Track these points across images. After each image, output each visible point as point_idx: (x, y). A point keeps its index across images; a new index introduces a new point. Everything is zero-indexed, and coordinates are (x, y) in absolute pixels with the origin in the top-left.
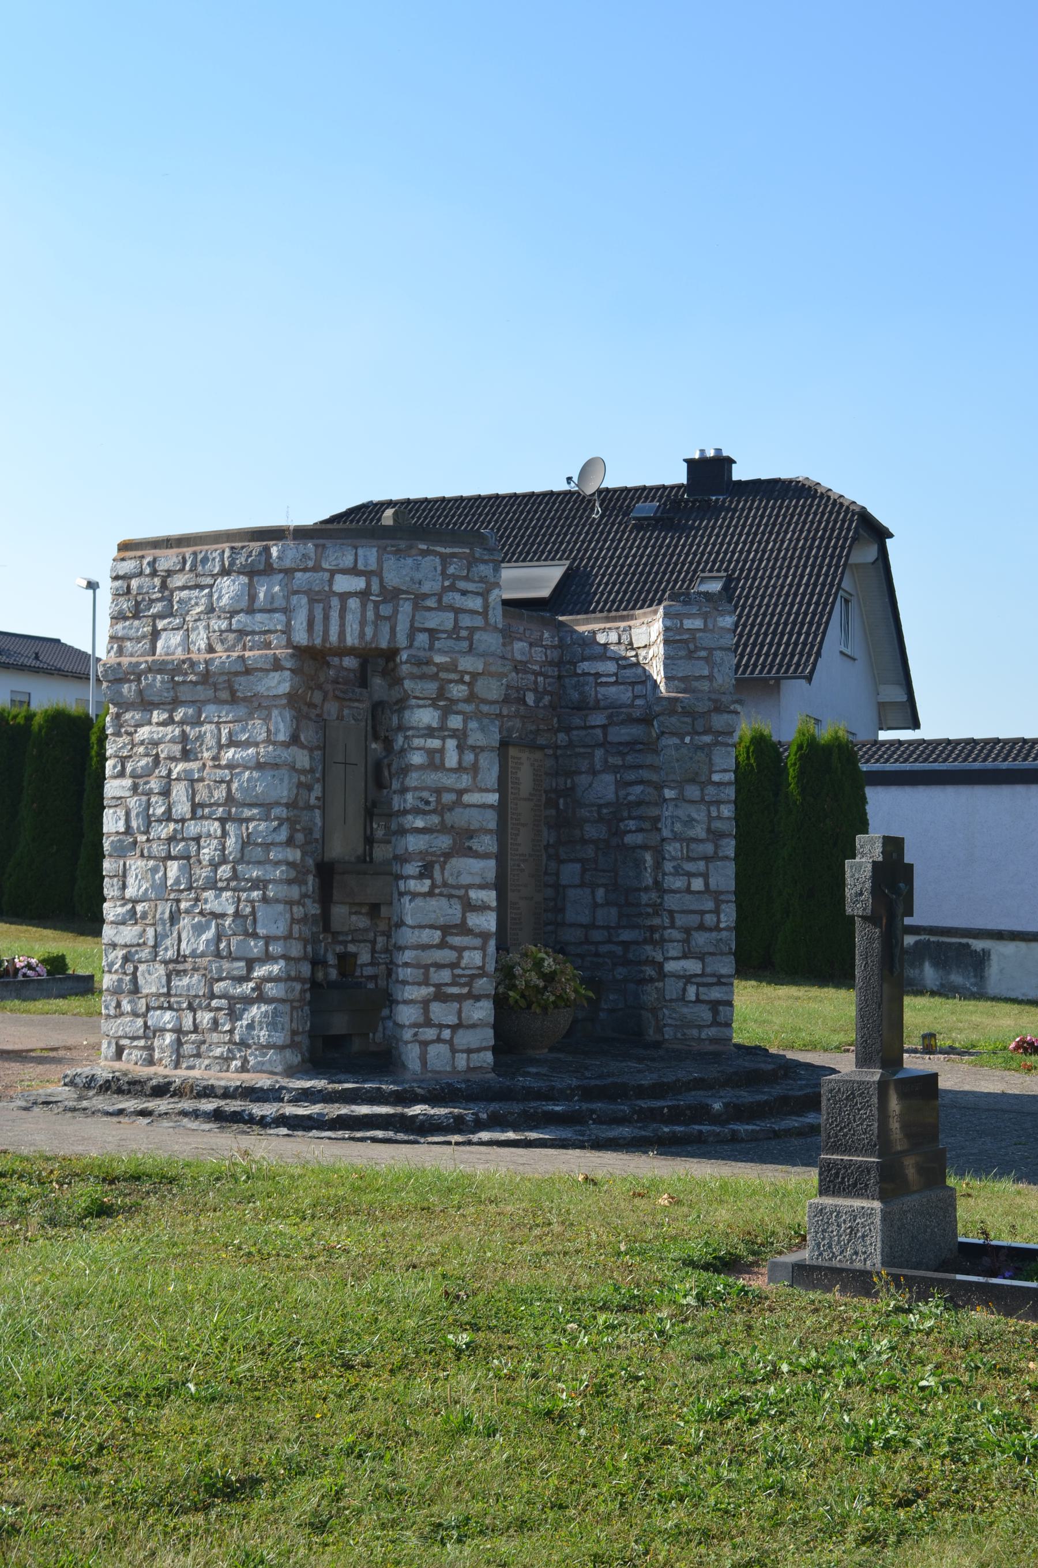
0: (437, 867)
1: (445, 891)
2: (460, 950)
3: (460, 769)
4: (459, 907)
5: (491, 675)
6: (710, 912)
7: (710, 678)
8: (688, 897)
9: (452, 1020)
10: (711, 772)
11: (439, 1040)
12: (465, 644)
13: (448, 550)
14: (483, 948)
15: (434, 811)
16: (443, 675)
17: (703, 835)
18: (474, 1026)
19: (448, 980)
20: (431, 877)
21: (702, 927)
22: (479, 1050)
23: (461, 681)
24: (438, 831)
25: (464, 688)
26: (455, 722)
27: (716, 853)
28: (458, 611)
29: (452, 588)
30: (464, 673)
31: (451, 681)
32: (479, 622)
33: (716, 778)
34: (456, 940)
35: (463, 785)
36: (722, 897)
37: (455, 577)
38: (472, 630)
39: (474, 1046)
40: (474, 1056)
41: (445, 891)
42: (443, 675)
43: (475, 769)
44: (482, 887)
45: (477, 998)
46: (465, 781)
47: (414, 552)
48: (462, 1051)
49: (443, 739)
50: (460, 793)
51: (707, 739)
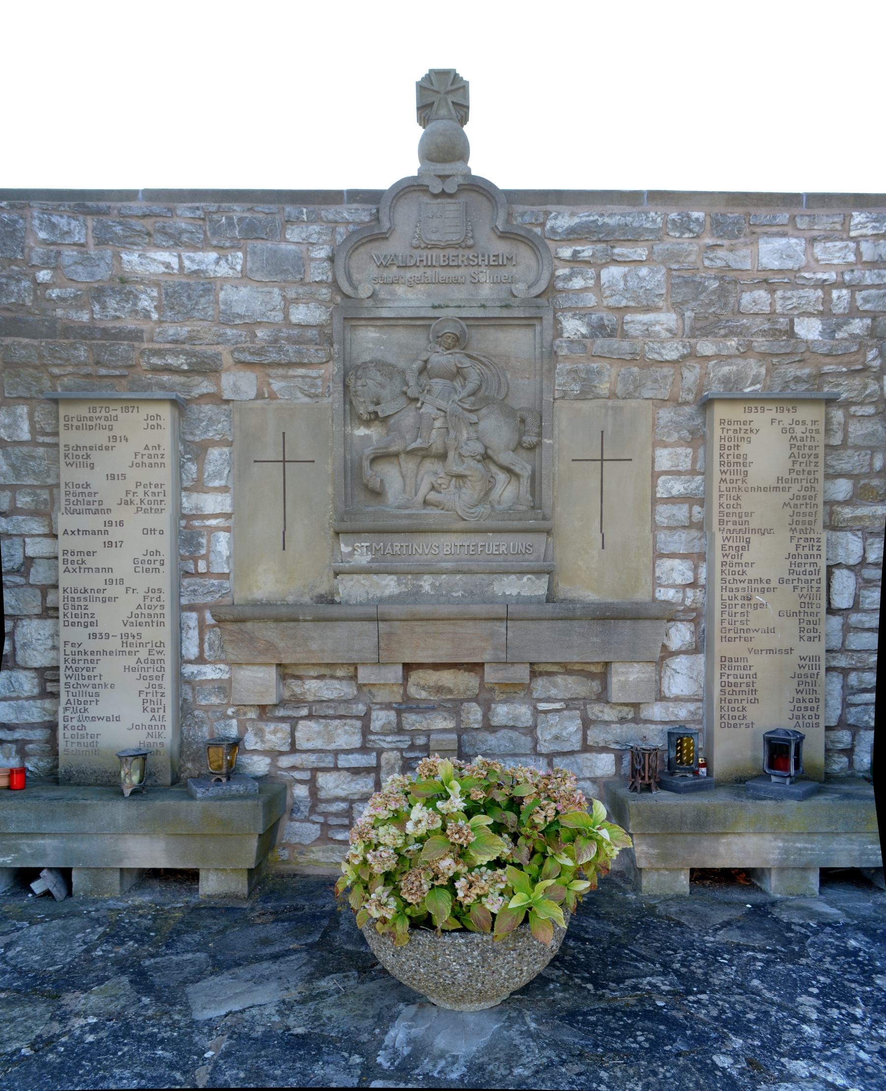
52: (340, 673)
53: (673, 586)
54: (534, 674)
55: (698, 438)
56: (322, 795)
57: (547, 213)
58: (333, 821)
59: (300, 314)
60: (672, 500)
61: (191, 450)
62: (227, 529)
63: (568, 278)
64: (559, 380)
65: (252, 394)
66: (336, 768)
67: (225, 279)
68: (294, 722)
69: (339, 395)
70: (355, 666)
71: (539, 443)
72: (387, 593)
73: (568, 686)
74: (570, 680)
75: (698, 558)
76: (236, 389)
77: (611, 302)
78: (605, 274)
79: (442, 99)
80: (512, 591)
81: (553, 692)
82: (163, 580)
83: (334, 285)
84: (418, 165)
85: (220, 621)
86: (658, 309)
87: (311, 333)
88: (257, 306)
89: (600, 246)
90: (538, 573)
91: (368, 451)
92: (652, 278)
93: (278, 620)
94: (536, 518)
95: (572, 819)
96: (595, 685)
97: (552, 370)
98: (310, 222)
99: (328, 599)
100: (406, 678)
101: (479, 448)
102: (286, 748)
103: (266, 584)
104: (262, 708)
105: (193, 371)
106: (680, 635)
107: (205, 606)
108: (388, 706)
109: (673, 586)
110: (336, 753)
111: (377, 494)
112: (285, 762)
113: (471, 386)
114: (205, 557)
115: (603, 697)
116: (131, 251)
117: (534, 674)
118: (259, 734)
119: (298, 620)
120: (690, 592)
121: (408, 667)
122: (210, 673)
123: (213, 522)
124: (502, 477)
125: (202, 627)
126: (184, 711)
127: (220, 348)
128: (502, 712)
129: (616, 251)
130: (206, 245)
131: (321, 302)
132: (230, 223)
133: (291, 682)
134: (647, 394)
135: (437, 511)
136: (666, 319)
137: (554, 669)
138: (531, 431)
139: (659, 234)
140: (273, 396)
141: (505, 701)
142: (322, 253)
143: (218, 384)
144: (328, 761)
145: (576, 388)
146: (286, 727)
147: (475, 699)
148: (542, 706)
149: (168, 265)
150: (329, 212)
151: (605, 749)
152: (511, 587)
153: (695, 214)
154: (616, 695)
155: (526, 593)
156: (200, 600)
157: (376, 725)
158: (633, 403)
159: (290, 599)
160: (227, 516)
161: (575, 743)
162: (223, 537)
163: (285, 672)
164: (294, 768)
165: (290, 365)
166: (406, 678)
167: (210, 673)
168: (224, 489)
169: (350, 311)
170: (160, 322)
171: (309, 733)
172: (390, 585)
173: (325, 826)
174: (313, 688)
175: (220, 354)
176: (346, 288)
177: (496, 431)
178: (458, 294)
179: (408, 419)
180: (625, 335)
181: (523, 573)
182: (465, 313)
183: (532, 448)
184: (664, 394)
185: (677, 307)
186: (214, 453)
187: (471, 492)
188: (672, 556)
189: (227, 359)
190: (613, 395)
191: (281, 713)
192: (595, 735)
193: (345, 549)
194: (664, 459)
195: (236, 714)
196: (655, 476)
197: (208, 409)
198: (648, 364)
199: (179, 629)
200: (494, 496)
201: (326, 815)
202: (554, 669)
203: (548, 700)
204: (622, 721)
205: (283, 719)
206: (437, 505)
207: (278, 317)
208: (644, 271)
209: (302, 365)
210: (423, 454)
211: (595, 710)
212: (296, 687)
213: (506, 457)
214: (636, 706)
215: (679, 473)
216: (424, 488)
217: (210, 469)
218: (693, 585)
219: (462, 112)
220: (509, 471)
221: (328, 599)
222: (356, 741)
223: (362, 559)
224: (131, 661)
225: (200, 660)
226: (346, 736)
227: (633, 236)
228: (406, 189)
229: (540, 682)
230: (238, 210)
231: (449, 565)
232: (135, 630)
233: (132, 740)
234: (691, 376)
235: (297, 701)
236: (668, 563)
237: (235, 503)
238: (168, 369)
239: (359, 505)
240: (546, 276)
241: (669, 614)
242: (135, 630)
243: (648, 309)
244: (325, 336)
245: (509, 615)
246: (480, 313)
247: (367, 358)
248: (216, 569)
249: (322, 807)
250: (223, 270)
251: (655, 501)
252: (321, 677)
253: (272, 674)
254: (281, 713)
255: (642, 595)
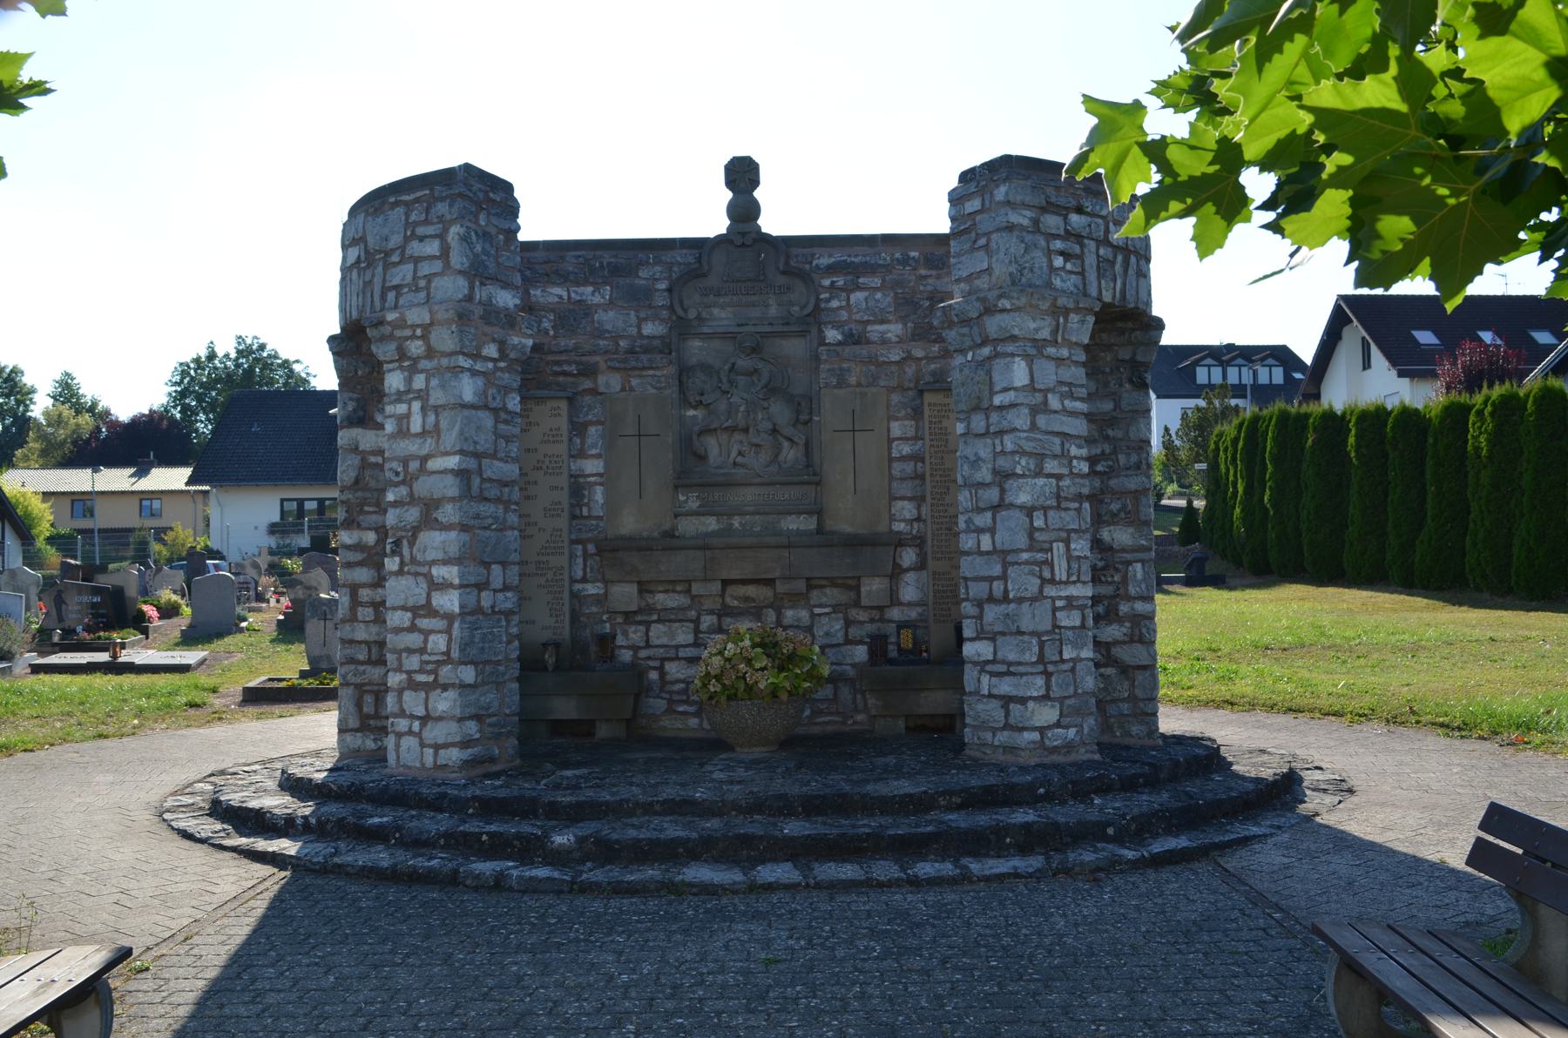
0: (405, 542)
1: (414, 569)
2: (427, 633)
3: (424, 434)
4: (425, 586)
5: (441, 324)
6: (998, 578)
7: (989, 271)
8: (979, 560)
9: (420, 711)
10: (992, 393)
11: (410, 732)
12: (423, 295)
13: (412, 197)
14: (448, 631)
15: (403, 482)
16: (398, 333)
17: (989, 478)
18: (440, 719)
19: (416, 666)
20: (402, 556)
21: (991, 599)
22: (446, 746)
23: (413, 337)
24: (409, 504)
25: (420, 343)
26: (419, 382)
27: (1002, 499)
28: (417, 260)
29: (414, 236)
30: (414, 327)
31: (407, 338)
32: (437, 266)
33: (997, 400)
34: (424, 623)
35: (424, 452)
36: (1009, 559)
37: (417, 224)
38: (429, 278)
39: (440, 741)
40: (442, 752)
41: (414, 569)
42: (398, 333)
43: (437, 430)
44: (446, 562)
45: (445, 688)
46: (428, 446)
47: (387, 207)
48: (430, 746)
49: (409, 402)
50: (424, 459)
51: (986, 351)
52: (679, 588)
53: (904, 520)
54: (810, 587)
55: (917, 414)
56: (668, 678)
57: (813, 255)
58: (676, 697)
59: (649, 329)
60: (903, 458)
61: (578, 429)
62: (601, 484)
63: (828, 300)
64: (823, 375)
65: (618, 388)
66: (678, 658)
67: (598, 305)
68: (648, 624)
69: (676, 389)
70: (689, 582)
71: (811, 420)
72: (710, 529)
73: (833, 595)
74: (835, 590)
75: (919, 500)
76: (607, 385)
77: (857, 317)
78: (853, 297)
79: (742, 174)
80: (793, 526)
81: (824, 600)
82: (563, 522)
83: (671, 308)
84: (728, 222)
85: (600, 552)
86: (889, 322)
87: (657, 343)
88: (620, 324)
89: (849, 277)
90: (810, 513)
91: (696, 429)
92: (884, 299)
93: (639, 549)
94: (811, 474)
95: (801, 651)
96: (852, 594)
97: (817, 370)
98: (655, 263)
99: (670, 534)
100: (724, 591)
101: (769, 426)
102: (642, 644)
103: (629, 524)
104: (627, 615)
105: (581, 374)
106: (908, 557)
107: (588, 541)
108: (711, 612)
109: (904, 520)
110: (677, 647)
111: (702, 458)
112: (643, 654)
113: (764, 381)
114: (587, 505)
115: (857, 604)
116: (536, 288)
117: (810, 587)
118: (625, 633)
119: (651, 549)
120: (915, 525)
121: (726, 583)
122: (592, 589)
123: (592, 479)
124: (786, 444)
125: (586, 556)
126: (575, 617)
127: (598, 358)
128: (789, 615)
129: (861, 280)
130: (586, 283)
131: (662, 320)
132: (602, 267)
133: (647, 596)
134: (882, 383)
135: (742, 471)
136: (894, 330)
137: (824, 582)
138: (804, 408)
139: (888, 268)
140: (632, 389)
141: (792, 607)
142: (663, 286)
143: (595, 381)
144: (672, 653)
145: (834, 381)
146: (642, 628)
147: (771, 606)
148: (817, 611)
149: (560, 297)
150: (668, 257)
151: (861, 642)
152: (792, 524)
153: (913, 254)
154: (865, 601)
155: (802, 527)
156: (584, 536)
157: (704, 626)
158: (874, 390)
159: (645, 534)
160: (600, 475)
161: (840, 638)
162: (599, 490)
163: (644, 588)
164: (649, 658)
165: (644, 368)
166: (724, 591)
167: (592, 589)
168: (598, 456)
169: (682, 328)
170: (555, 337)
171: (658, 633)
172: (712, 524)
173: (671, 701)
174: (662, 599)
175: (597, 363)
176: (680, 312)
177: (780, 412)
178: (755, 313)
179: (722, 406)
180: (868, 342)
181: (801, 513)
182: (759, 329)
183: (806, 423)
184: (894, 383)
185: (903, 319)
186: (592, 430)
187: (764, 457)
188: (902, 498)
189: (603, 366)
190: (859, 385)
191: (639, 618)
192: (854, 632)
193: (682, 498)
194: (896, 429)
195: (609, 619)
196: (890, 441)
197: (588, 399)
198: (880, 365)
199: (572, 556)
200: (781, 458)
201: (671, 693)
202: (824, 582)
203: (820, 606)
204: (872, 621)
205: (640, 623)
206: (743, 466)
207: (633, 331)
208: (879, 295)
209: (651, 368)
210: (732, 429)
211: (854, 613)
212: (650, 599)
213: (788, 431)
214: (881, 609)
215: (907, 439)
216: (734, 454)
217: (589, 441)
218: (918, 519)
219: (755, 183)
220: (790, 440)
221: (670, 534)
222: (690, 638)
223: (693, 504)
224: (542, 581)
225: (584, 580)
226: (684, 636)
227: (870, 269)
228: (720, 239)
229: (815, 593)
230: (607, 257)
231: (751, 509)
232: (545, 559)
233: (546, 636)
234: (910, 370)
235: (650, 609)
236: (900, 504)
237: (606, 467)
238: (565, 373)
239: (690, 470)
240: (812, 301)
241: (900, 542)
242: (545, 559)
243: (882, 322)
244: (666, 347)
245: (791, 543)
246: (768, 329)
247: (694, 361)
248: (595, 513)
249: (668, 687)
250: (597, 299)
251: (891, 460)
252: (666, 591)
253: (632, 589)
254: (639, 618)
255: (882, 528)
